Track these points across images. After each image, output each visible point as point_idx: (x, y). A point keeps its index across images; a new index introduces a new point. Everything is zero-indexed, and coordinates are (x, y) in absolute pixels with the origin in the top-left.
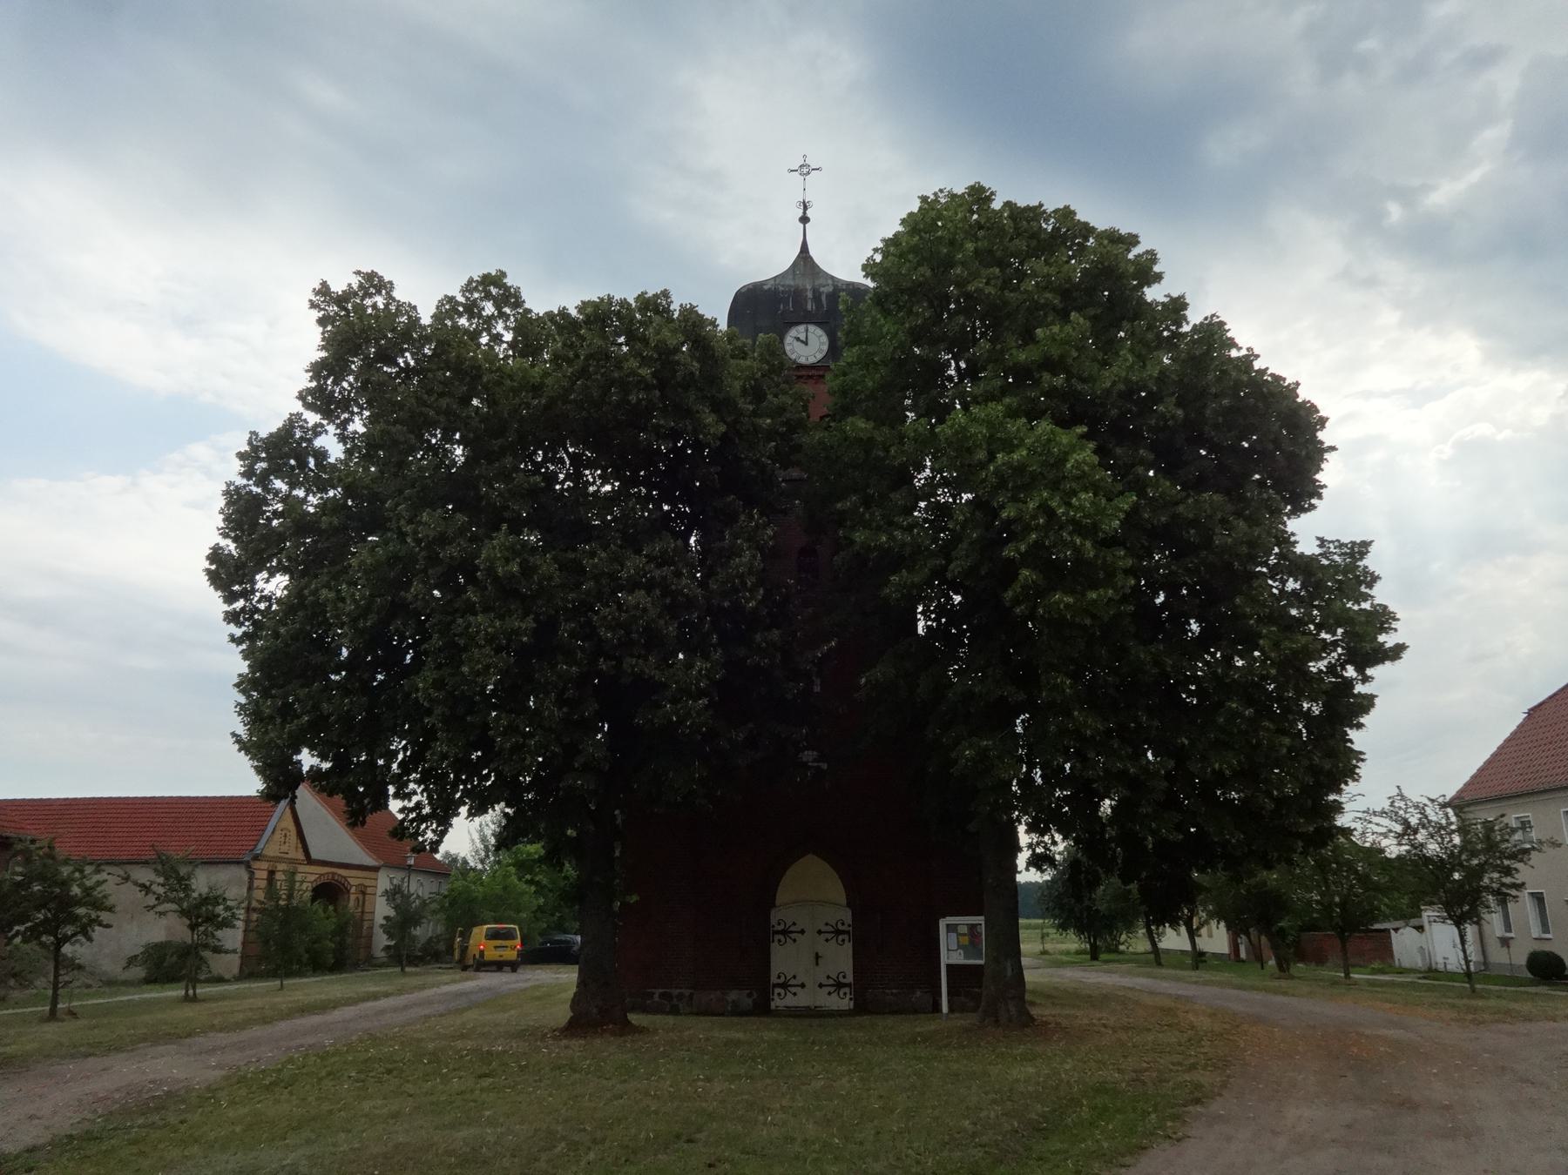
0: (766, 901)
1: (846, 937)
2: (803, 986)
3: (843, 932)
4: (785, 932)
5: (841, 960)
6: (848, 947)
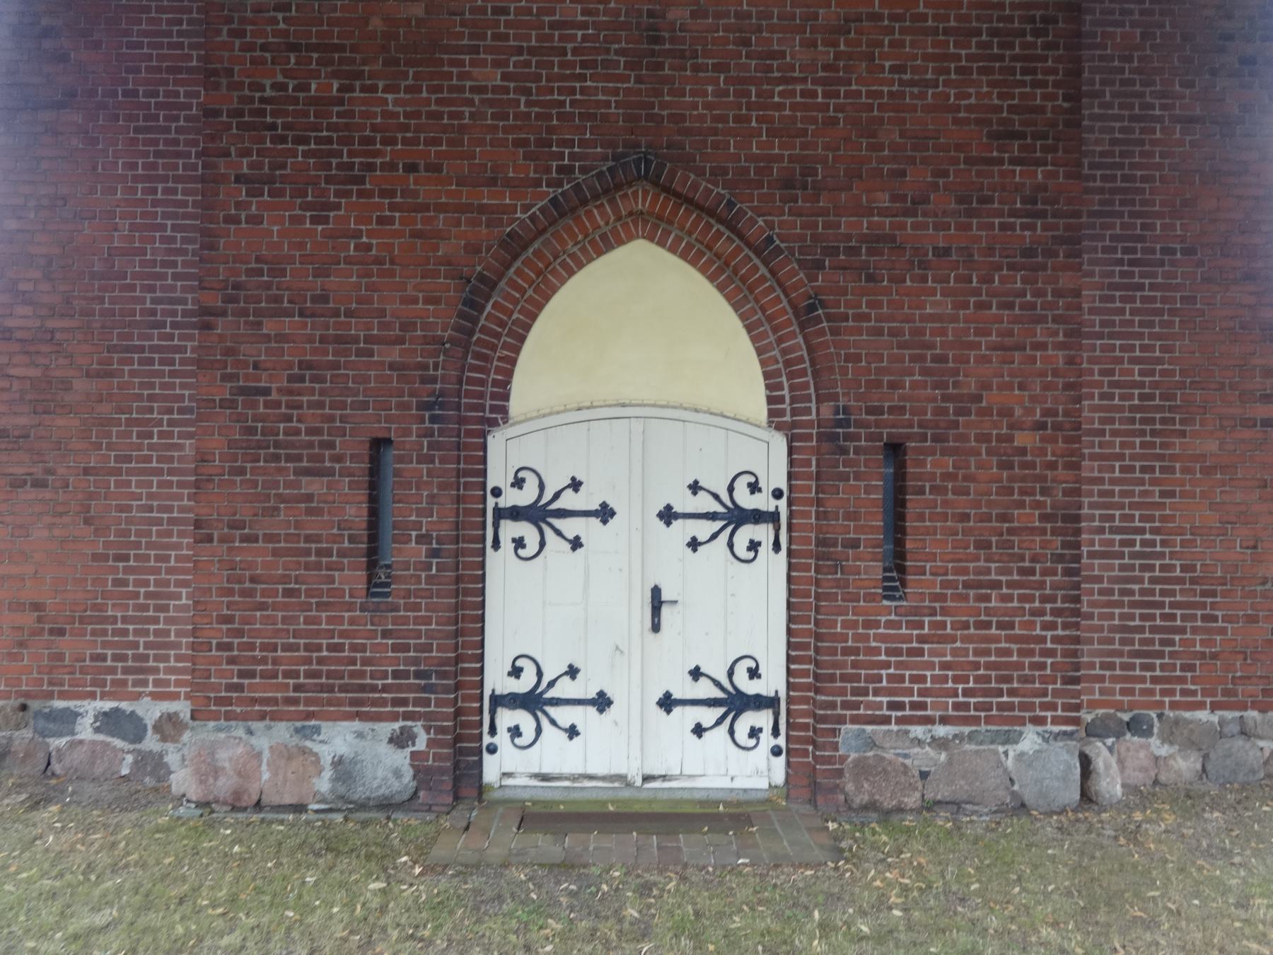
0: (470, 396)
1: (763, 533)
2: (602, 702)
3: (757, 517)
4: (538, 514)
5: (743, 610)
6: (773, 567)
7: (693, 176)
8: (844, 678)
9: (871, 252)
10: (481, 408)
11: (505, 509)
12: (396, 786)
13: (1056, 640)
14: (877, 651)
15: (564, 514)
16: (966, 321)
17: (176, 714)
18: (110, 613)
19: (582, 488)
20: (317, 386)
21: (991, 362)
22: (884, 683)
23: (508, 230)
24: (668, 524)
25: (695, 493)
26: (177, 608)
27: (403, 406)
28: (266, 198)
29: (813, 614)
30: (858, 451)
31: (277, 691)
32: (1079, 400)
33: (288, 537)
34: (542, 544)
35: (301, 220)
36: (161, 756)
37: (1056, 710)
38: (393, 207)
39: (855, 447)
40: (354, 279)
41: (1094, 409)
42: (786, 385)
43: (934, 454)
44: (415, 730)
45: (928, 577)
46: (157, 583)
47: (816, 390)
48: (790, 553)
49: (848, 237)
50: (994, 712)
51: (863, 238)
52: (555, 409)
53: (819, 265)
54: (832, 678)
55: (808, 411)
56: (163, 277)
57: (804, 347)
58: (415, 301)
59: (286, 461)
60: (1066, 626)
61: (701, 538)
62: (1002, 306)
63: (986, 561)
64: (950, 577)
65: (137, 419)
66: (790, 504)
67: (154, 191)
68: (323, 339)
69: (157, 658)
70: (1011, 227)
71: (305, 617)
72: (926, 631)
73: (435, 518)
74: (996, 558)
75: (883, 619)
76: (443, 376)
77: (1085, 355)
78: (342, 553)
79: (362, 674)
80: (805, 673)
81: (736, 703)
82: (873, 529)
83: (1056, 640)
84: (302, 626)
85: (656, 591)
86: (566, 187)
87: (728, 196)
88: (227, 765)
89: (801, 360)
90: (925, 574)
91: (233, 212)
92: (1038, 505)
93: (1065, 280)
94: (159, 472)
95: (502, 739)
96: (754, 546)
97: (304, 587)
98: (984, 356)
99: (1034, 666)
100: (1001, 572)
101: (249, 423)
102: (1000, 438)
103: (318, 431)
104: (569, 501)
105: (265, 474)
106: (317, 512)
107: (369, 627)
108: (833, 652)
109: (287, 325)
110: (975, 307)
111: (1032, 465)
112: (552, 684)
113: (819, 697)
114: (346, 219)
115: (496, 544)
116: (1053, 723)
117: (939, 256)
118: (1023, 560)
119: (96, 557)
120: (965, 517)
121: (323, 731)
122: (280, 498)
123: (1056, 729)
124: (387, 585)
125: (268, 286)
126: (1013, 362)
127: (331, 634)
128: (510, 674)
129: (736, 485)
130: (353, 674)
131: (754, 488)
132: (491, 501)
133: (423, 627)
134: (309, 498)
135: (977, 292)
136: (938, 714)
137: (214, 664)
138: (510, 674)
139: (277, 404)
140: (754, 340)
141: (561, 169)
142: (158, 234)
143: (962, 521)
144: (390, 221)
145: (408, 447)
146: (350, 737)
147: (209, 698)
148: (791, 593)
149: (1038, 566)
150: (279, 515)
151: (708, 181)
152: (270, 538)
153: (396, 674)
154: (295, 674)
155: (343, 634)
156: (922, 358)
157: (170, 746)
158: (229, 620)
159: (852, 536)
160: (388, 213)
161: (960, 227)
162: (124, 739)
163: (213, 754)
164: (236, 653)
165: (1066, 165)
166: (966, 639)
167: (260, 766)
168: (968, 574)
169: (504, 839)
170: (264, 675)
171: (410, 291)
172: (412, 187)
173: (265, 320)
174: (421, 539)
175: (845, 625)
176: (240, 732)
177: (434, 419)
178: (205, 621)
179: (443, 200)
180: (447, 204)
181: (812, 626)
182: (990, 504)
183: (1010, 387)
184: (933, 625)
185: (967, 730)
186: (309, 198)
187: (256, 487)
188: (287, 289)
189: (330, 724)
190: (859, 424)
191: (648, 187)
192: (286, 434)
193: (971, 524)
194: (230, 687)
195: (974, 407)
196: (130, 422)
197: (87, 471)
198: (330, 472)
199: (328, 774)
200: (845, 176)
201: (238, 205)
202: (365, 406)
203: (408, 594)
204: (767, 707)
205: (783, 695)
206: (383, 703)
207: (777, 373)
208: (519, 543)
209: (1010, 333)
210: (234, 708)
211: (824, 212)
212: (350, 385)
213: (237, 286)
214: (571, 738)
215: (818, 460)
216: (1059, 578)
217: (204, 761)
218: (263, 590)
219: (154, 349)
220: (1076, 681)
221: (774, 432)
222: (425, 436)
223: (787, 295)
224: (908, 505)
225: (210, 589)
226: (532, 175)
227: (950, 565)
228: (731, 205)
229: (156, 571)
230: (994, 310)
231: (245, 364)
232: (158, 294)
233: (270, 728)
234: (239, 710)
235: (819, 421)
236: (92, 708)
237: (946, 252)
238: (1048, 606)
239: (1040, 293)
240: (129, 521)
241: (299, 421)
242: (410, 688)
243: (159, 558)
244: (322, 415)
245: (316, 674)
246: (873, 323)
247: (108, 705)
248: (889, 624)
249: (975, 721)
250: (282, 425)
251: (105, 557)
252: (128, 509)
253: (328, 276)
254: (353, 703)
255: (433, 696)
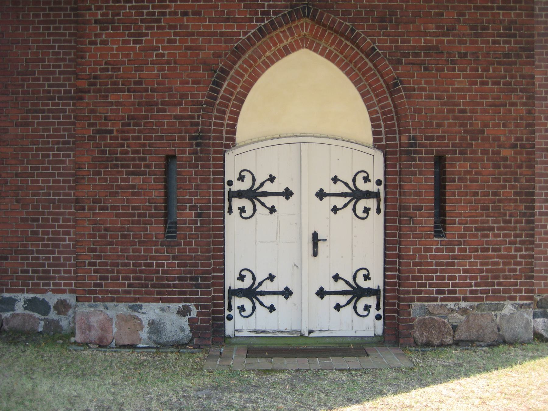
0: (213, 134)
1: (371, 203)
3: (368, 195)
4: (252, 195)
5: (359, 244)
6: (376, 222)
7: (333, 16)
8: (414, 278)
9: (426, 55)
10: (221, 138)
11: (235, 192)
12: (182, 335)
13: (522, 257)
14: (431, 264)
15: (266, 194)
16: (476, 91)
17: (65, 300)
18: (30, 248)
19: (276, 180)
20: (137, 128)
21: (489, 113)
22: (435, 281)
23: (236, 45)
24: (321, 199)
25: (335, 183)
26: (64, 246)
27: (182, 138)
28: (110, 31)
29: (398, 245)
30: (421, 159)
31: (120, 287)
32: (533, 132)
33: (123, 208)
34: (255, 210)
35: (128, 42)
36: (58, 322)
37: (521, 293)
38: (175, 34)
39: (419, 157)
40: (156, 72)
41: (542, 137)
42: (383, 125)
43: (460, 161)
44: (191, 307)
45: (457, 225)
46: (53, 233)
47: (399, 127)
48: (385, 214)
49: (414, 48)
50: (490, 294)
51: (422, 48)
52: (260, 139)
53: (399, 62)
54: (408, 278)
55: (394, 139)
56: (54, 73)
57: (392, 105)
58: (187, 83)
59: (122, 168)
60: (527, 250)
61: (339, 206)
62: (494, 83)
63: (487, 216)
64: (468, 225)
65: (41, 147)
66: (385, 188)
67: (49, 29)
68: (140, 104)
69: (55, 272)
70: (498, 42)
71: (133, 249)
72: (456, 253)
73: (199, 197)
74: (492, 215)
75: (434, 247)
76: (202, 122)
77: (537, 109)
78: (151, 215)
79: (162, 278)
80: (394, 277)
81: (357, 293)
82: (429, 201)
83: (522, 257)
84: (131, 254)
85: (315, 235)
86: (266, 22)
87: (351, 26)
88: (95, 324)
89: (390, 112)
90: (455, 224)
91: (93, 39)
92: (512, 187)
93: (526, 70)
94: (53, 175)
95: (235, 312)
96: (366, 210)
97: (132, 233)
98: (485, 110)
99: (511, 270)
100: (494, 222)
101: (103, 148)
102: (494, 153)
103: (137, 152)
104: (268, 187)
105: (110, 175)
106: (139, 194)
107: (166, 254)
108: (408, 265)
109: (121, 97)
110: (480, 84)
111: (510, 166)
112: (260, 284)
113: (401, 288)
114: (151, 41)
115: (230, 211)
116: (520, 299)
117: (461, 57)
118: (505, 216)
119: (22, 220)
120: (476, 194)
121: (143, 307)
122: (119, 187)
123: (521, 302)
124: (175, 232)
125: (111, 77)
126: (500, 113)
127: (146, 258)
128: (238, 279)
129: (357, 178)
130: (158, 278)
131: (366, 179)
132: (227, 188)
133: (194, 254)
134: (134, 187)
135: (481, 76)
136: (462, 296)
137: (87, 273)
138: (238, 279)
139: (116, 138)
140: (365, 101)
141: (263, 13)
142: (51, 51)
143: (474, 196)
144: (174, 41)
145: (184, 159)
146: (158, 311)
147: (85, 290)
148: (386, 235)
149: (513, 219)
150: (118, 196)
151: (340, 18)
152: (114, 208)
153: (180, 279)
154: (128, 279)
155: (152, 258)
156: (453, 111)
157: (62, 317)
158: (94, 250)
159: (418, 204)
160: (173, 37)
161: (472, 42)
162: (39, 313)
163: (88, 319)
164: (98, 267)
165: (526, 10)
166: (477, 257)
167: (112, 325)
168: (477, 223)
169: (238, 360)
170: (113, 279)
171: (185, 78)
172: (186, 24)
173: (110, 94)
174: (192, 208)
175: (415, 251)
176: (101, 308)
177: (198, 145)
178: (82, 251)
179: (202, 30)
180: (204, 32)
181: (397, 252)
182: (489, 187)
183: (498, 125)
184: (460, 250)
185: (476, 304)
186: (132, 31)
187: (107, 182)
188: (121, 78)
189: (147, 304)
190: (421, 145)
191: (309, 21)
192: (121, 153)
193: (479, 197)
194: (96, 285)
195: (480, 136)
196: (38, 149)
197: (17, 175)
198: (144, 173)
199: (146, 329)
200: (412, 16)
201: (96, 35)
202: (161, 138)
203: (185, 237)
204: (374, 295)
205: (382, 288)
206: (174, 293)
207: (378, 119)
208: (242, 210)
209: (498, 98)
210: (98, 296)
211: (402, 34)
212: (154, 127)
213: (95, 77)
214: (271, 312)
215: (400, 165)
216: (524, 225)
217: (84, 322)
218: (111, 235)
219: (49, 111)
220: (532, 277)
221: (376, 150)
222: (193, 154)
223: (382, 78)
224: (447, 187)
225: (84, 234)
226: (248, 16)
227: (468, 219)
228: (352, 31)
229: (53, 227)
230: (490, 86)
231: (100, 118)
232: (51, 82)
233: (116, 306)
234: (100, 296)
235: (400, 144)
236: (22, 297)
237: (465, 55)
238: (518, 239)
239: (512, 77)
240: (39, 201)
241: (128, 147)
242: (188, 286)
243: (54, 220)
244: (140, 143)
245: (139, 279)
246: (428, 92)
247: (30, 296)
248: (437, 250)
249: (481, 299)
250: (119, 149)
251: (27, 220)
252: (38, 194)
253: (142, 71)
254: (158, 293)
255: (199, 290)
